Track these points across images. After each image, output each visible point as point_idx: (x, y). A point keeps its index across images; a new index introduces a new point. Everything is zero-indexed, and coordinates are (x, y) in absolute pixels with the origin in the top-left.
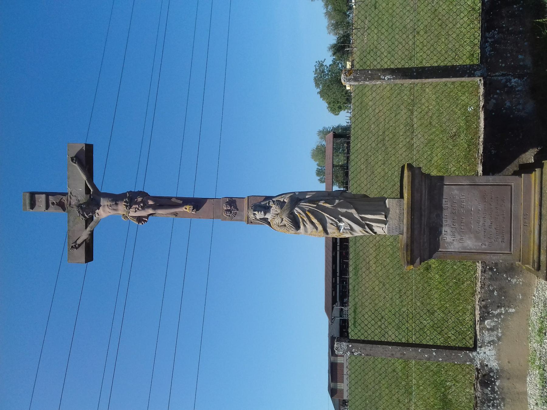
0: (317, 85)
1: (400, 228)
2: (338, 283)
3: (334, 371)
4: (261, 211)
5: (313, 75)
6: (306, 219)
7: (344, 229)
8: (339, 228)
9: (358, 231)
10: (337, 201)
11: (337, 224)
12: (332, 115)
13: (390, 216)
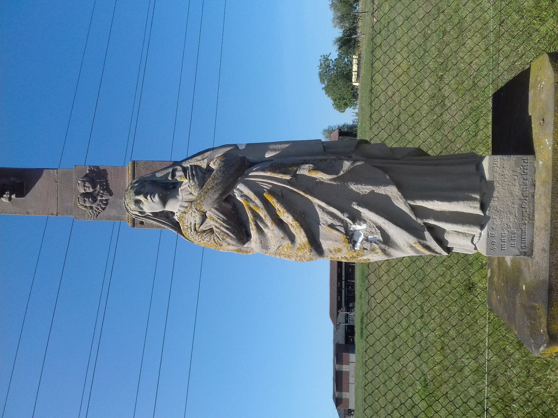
0: (322, 81)
1: (522, 239)
2: (343, 287)
3: (340, 380)
4: (152, 194)
5: (318, 70)
6: (262, 213)
7: (367, 239)
8: (351, 237)
9: (405, 244)
10: (347, 165)
11: (346, 226)
12: (337, 112)
13: (494, 203)
